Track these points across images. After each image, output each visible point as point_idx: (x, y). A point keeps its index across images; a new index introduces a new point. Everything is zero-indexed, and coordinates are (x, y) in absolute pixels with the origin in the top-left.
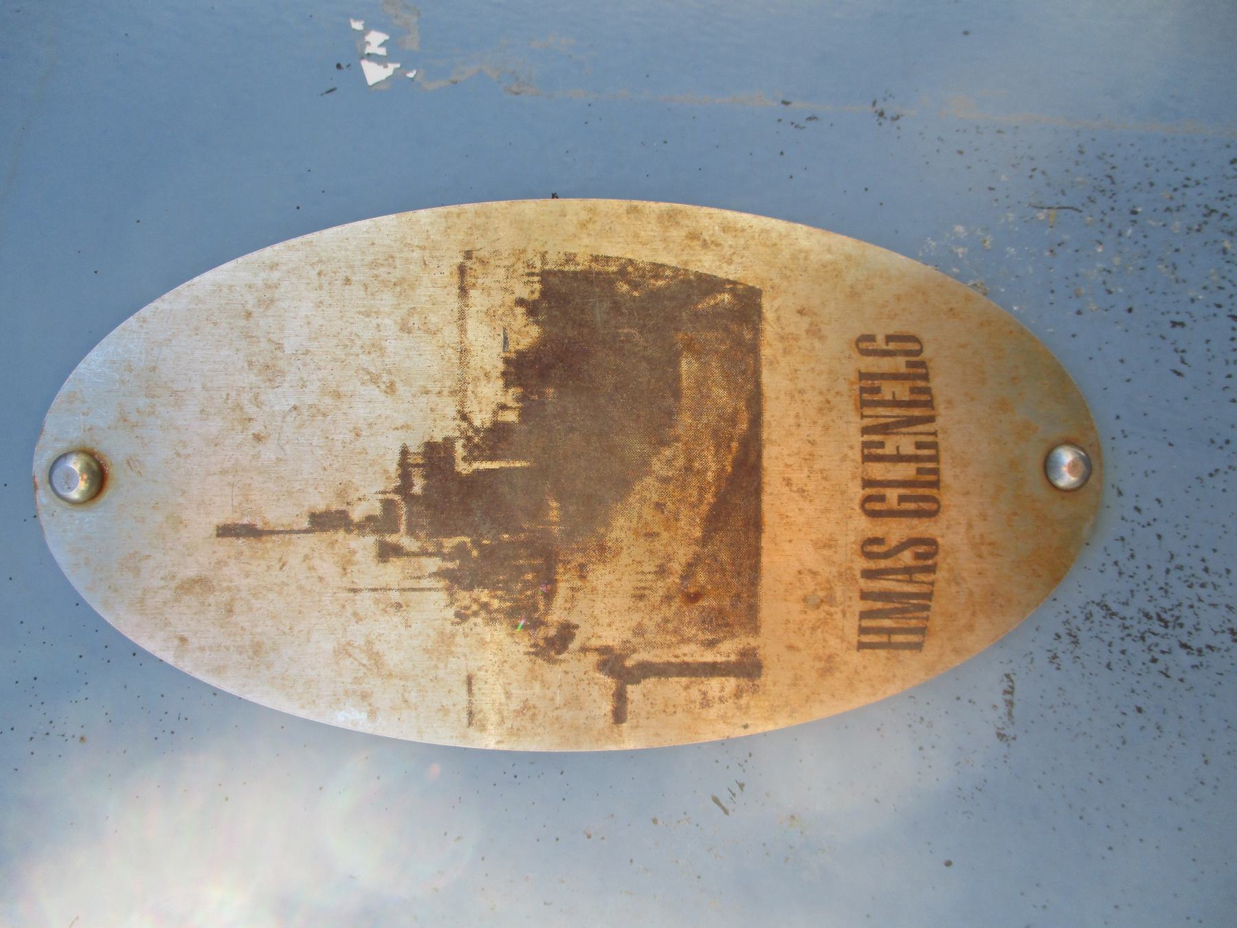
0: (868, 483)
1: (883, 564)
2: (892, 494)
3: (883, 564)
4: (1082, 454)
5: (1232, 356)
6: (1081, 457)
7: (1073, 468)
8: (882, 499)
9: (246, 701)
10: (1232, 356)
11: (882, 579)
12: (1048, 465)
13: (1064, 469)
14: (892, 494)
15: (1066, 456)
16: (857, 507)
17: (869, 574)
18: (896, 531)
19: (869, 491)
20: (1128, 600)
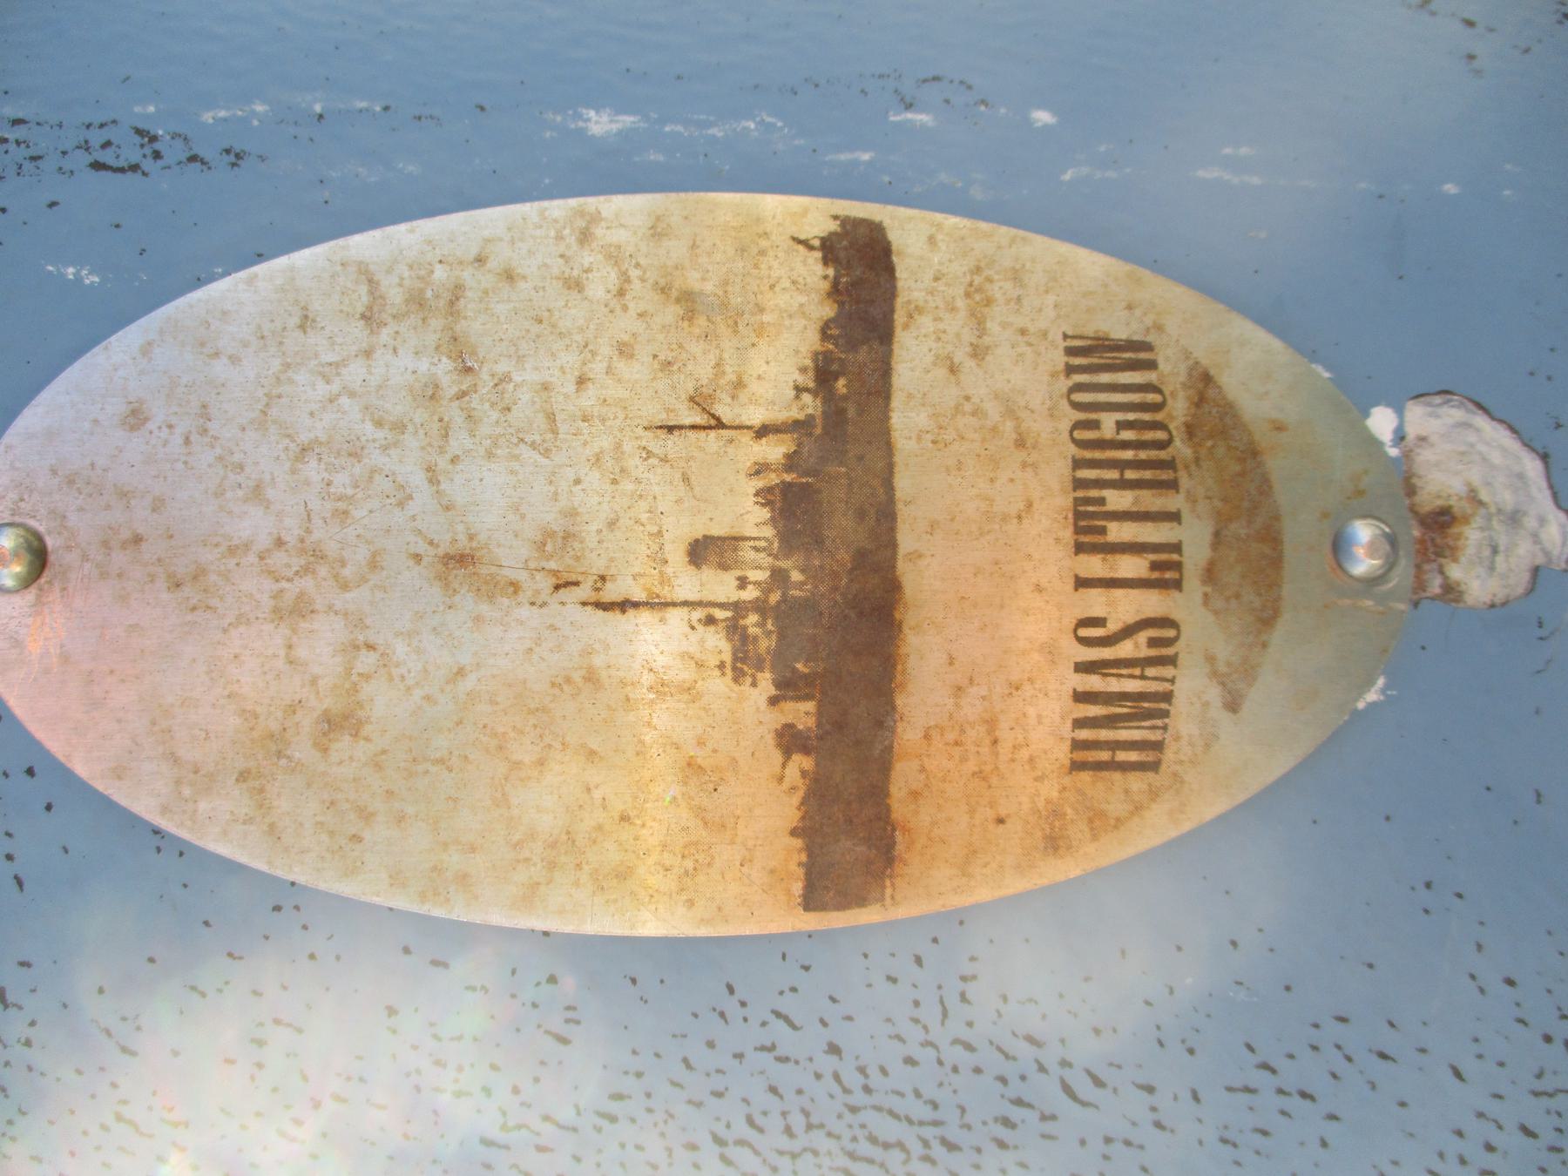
0: (1079, 484)
1: (1106, 653)
2: (1108, 421)
3: (1106, 653)
4: (1387, 530)
5: (1562, 1030)
6: (1385, 535)
7: (1372, 550)
8: (1095, 425)
9: (317, 892)
10: (1562, 1030)
11: (1091, 338)
12: (1339, 546)
13: (1360, 552)
14: (1108, 421)
15: (1363, 532)
16: (1066, 435)
17: (1084, 668)
18: (1124, 607)
19: (1080, 494)
20: (1556, 423)
